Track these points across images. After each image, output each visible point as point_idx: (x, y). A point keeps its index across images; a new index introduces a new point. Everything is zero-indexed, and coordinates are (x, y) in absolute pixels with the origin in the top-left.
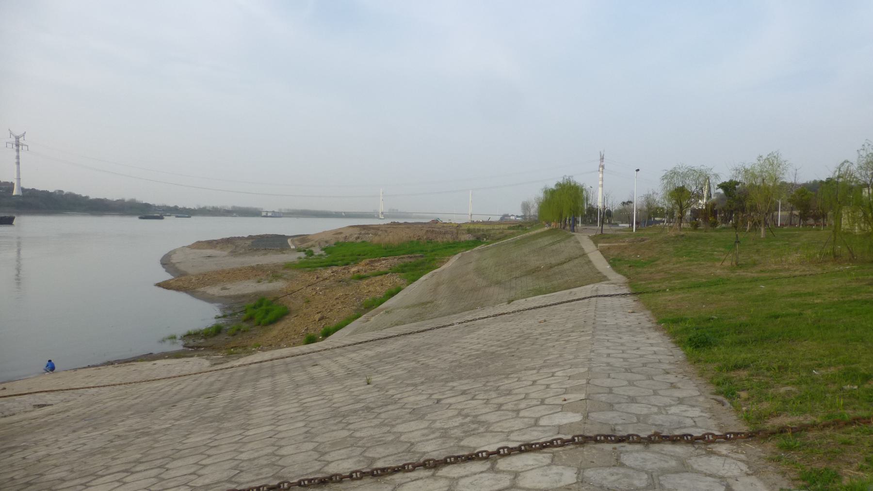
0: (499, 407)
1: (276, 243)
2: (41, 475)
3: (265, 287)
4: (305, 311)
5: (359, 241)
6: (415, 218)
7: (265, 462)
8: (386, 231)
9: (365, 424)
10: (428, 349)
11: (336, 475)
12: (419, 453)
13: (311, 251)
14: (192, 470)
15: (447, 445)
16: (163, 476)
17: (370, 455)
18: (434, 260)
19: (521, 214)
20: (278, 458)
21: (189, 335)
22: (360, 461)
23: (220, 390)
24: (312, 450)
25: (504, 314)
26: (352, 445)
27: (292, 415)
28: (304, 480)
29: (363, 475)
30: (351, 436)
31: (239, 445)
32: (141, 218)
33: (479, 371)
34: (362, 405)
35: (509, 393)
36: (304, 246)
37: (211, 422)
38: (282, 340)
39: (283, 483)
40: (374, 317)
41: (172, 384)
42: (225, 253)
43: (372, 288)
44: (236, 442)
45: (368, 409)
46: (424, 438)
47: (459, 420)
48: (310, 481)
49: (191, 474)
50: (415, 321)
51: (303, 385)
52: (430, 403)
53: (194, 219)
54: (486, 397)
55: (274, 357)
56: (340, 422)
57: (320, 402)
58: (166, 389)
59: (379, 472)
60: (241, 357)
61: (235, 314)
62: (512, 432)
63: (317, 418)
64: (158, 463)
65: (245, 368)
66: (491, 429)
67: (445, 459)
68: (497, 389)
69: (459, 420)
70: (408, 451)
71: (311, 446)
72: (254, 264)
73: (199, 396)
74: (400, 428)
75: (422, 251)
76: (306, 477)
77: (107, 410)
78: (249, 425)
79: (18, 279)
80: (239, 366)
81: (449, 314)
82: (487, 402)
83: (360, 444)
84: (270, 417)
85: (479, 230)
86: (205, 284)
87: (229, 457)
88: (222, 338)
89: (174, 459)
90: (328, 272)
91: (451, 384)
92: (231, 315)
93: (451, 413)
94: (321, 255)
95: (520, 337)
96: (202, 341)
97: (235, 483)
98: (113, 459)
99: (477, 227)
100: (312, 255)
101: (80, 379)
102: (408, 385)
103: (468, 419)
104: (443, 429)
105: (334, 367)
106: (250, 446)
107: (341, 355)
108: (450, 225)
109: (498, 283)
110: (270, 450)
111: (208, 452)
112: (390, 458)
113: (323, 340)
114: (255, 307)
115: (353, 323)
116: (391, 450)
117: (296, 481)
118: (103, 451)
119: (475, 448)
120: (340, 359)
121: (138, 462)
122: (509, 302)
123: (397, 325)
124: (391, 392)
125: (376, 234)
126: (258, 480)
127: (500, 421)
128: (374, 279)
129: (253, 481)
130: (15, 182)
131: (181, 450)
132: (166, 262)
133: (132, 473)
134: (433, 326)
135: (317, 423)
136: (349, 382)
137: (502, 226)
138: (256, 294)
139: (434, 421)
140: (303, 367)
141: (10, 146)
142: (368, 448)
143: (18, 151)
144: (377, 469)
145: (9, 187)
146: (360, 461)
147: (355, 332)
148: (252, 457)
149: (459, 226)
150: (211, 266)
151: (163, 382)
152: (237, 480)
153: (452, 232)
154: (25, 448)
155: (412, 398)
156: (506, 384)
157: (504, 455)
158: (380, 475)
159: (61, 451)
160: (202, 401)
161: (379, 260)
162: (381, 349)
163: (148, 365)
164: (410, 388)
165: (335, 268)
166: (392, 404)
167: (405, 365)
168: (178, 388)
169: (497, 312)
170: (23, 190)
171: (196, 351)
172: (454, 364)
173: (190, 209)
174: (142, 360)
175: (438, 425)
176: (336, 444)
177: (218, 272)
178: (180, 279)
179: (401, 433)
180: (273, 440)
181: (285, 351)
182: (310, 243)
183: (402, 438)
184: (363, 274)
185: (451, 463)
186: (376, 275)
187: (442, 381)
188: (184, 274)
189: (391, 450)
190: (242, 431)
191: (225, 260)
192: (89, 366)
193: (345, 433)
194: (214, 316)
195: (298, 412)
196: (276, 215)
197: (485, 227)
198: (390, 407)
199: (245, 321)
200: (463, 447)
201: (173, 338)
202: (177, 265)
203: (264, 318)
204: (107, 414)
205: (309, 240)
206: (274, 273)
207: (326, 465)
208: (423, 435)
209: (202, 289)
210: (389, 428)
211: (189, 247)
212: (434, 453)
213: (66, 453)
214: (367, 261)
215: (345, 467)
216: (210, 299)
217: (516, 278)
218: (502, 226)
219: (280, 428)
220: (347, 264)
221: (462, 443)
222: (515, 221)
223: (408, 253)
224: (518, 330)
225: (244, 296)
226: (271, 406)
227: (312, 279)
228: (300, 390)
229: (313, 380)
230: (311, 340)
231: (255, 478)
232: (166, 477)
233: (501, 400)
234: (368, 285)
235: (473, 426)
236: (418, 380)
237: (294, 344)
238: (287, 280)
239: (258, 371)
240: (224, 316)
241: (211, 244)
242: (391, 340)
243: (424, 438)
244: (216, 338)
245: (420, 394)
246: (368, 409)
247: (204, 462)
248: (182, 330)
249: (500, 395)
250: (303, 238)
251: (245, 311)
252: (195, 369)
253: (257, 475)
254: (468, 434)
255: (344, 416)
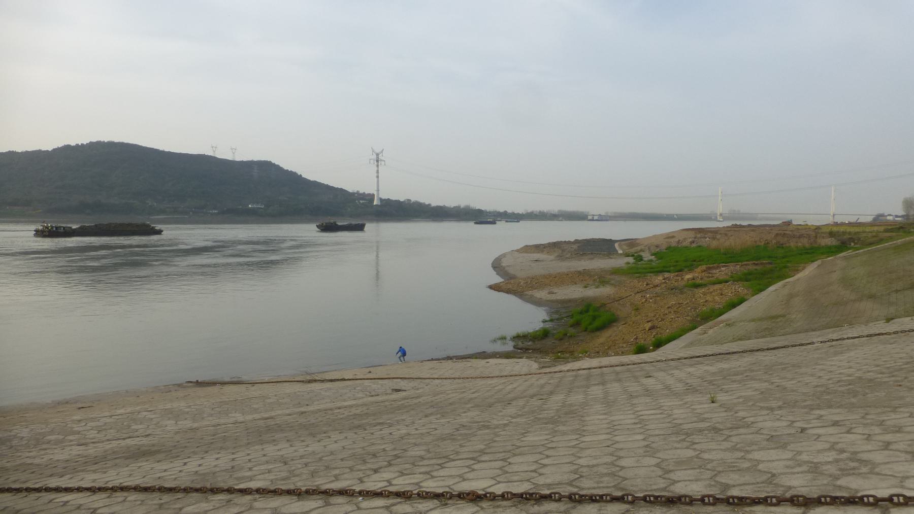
0: (887, 446)
1: (604, 247)
2: (405, 450)
3: (592, 292)
4: (634, 319)
5: (694, 245)
6: (760, 219)
7: (605, 471)
8: (726, 235)
9: (713, 445)
10: (783, 369)
11: (686, 496)
12: (782, 486)
13: (641, 256)
14: (533, 468)
15: (819, 482)
16: (506, 469)
17: (723, 481)
18: (785, 267)
19: (902, 213)
20: (618, 469)
21: (517, 337)
22: (710, 486)
23: (551, 393)
24: (655, 466)
25: (883, 334)
26: (700, 467)
27: (629, 427)
28: (649, 496)
29: (717, 501)
30: (697, 457)
31: (575, 450)
32: (476, 223)
33: (854, 400)
34: (708, 424)
35: (899, 430)
36: (633, 250)
37: (546, 424)
38: (609, 348)
39: (627, 495)
40: (712, 330)
41: (504, 383)
42: (552, 257)
43: (712, 297)
44: (573, 447)
45: (716, 430)
46: (788, 471)
47: (831, 456)
48: (656, 497)
49: (531, 471)
50: (763, 337)
51: (637, 397)
52: (793, 431)
53: (522, 223)
54: (866, 432)
55: (603, 364)
56: (684, 440)
57: (658, 416)
58: (500, 387)
59: (736, 501)
60: (569, 362)
61: (562, 318)
62: (908, 477)
63: (657, 432)
64: (501, 456)
65: (574, 373)
66: (877, 470)
67: (819, 498)
68: (881, 423)
69: (831, 456)
70: (769, 482)
71: (654, 461)
72: (580, 269)
73: (532, 397)
74: (757, 455)
75: (770, 257)
76: (650, 493)
77: (451, 401)
78: (584, 431)
79: (378, 276)
80: (568, 371)
81: (807, 331)
82: (869, 437)
83: (709, 466)
84: (605, 426)
85: (844, 233)
86: (533, 288)
87: (568, 461)
88: (549, 342)
89: (515, 455)
90: (659, 279)
91: (818, 412)
92: (558, 319)
93: (820, 446)
94: (651, 261)
95: (908, 363)
96: (530, 343)
97: (577, 487)
98: (461, 446)
99: (842, 229)
100: (642, 260)
101: (425, 370)
102: (762, 408)
103: (844, 456)
104: (812, 463)
105: (670, 381)
106: (588, 452)
107: (676, 368)
108: (806, 227)
109: (872, 297)
110: (609, 459)
111: (546, 453)
112: (747, 487)
113: (654, 350)
114: (581, 313)
115: (687, 335)
116: (747, 478)
117: (642, 495)
118: (451, 437)
119: (857, 491)
120: (676, 372)
121: (483, 452)
122: (888, 320)
123: (740, 339)
124: (741, 414)
125: (714, 238)
126: (599, 488)
127: (888, 463)
128: (712, 288)
129: (594, 488)
130: (375, 193)
131: (520, 447)
132: (497, 265)
133: (479, 462)
134: (786, 343)
135: (657, 439)
136: (689, 398)
137: (876, 228)
138: (583, 300)
139: (800, 453)
140: (636, 377)
141: (372, 161)
142: (719, 472)
143: (378, 166)
144: (733, 497)
145: (372, 196)
146: (710, 486)
147: (691, 344)
148: (591, 464)
149: (818, 228)
150: (538, 270)
151: (495, 381)
152: (578, 484)
153: (809, 236)
154: (391, 425)
155: (768, 424)
156: (892, 419)
157: (899, 504)
158: (738, 505)
159: (417, 432)
160: (535, 402)
161: (718, 267)
162: (725, 365)
163: (482, 363)
164: (765, 412)
165: (667, 275)
166: (743, 427)
167: (756, 385)
168: (510, 387)
169: (872, 332)
170: (381, 200)
171: (525, 352)
172: (819, 389)
173: (518, 214)
174: (476, 358)
175: (804, 457)
176: (681, 463)
177: (545, 277)
178: (510, 283)
179: (759, 462)
180: (611, 450)
181: (614, 360)
182: (639, 248)
183: (761, 467)
184: (698, 281)
185: (826, 504)
186: (714, 284)
187: (805, 407)
188: (513, 277)
189: (747, 478)
190: (577, 436)
191: (551, 264)
192: (432, 360)
193: (690, 453)
194: (541, 319)
195: (635, 423)
196: (602, 218)
197: (853, 230)
198: (742, 431)
199: (571, 326)
200: (840, 487)
201: (503, 338)
202: (507, 269)
203: (591, 324)
204: (451, 404)
205: (638, 245)
206: (601, 278)
207: (673, 484)
208: (787, 467)
209: (530, 293)
210: (743, 454)
211: (517, 251)
212: (803, 489)
213: (422, 434)
214: (704, 267)
215: (696, 489)
216: (538, 303)
217: (897, 291)
218: (876, 228)
219: (617, 439)
220: (680, 271)
221: (839, 483)
222: (895, 222)
223: (752, 260)
224: (904, 355)
225: (570, 301)
226: (605, 414)
227: (641, 285)
228: (635, 401)
229: (648, 392)
230: (641, 350)
231: (596, 485)
232: (510, 470)
233: (888, 437)
234: (704, 294)
235: (852, 464)
236: (774, 404)
237: (623, 353)
238: (615, 286)
239: (588, 378)
240: (551, 320)
241: (539, 248)
242: (735, 356)
243: (788, 471)
244: (544, 342)
245: (778, 419)
246: (716, 430)
247: (543, 462)
248: (512, 332)
249: (886, 431)
250: (631, 243)
251: (572, 316)
252: (525, 370)
253: (598, 482)
254: (846, 472)
255: (688, 435)
